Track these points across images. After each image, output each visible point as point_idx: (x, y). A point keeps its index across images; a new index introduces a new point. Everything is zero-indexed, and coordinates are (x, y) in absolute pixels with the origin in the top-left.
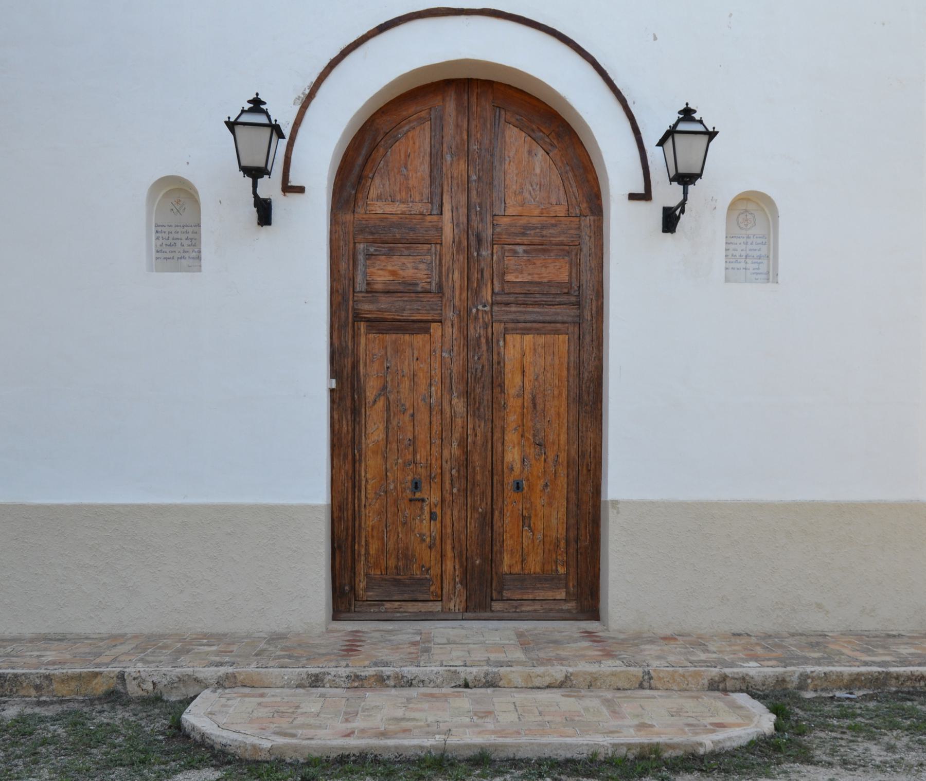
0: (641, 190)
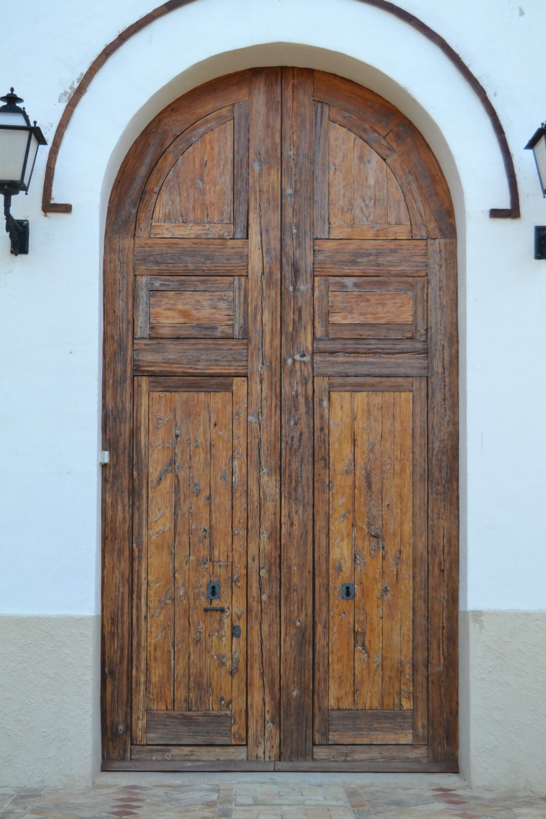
0: (505, 204)
